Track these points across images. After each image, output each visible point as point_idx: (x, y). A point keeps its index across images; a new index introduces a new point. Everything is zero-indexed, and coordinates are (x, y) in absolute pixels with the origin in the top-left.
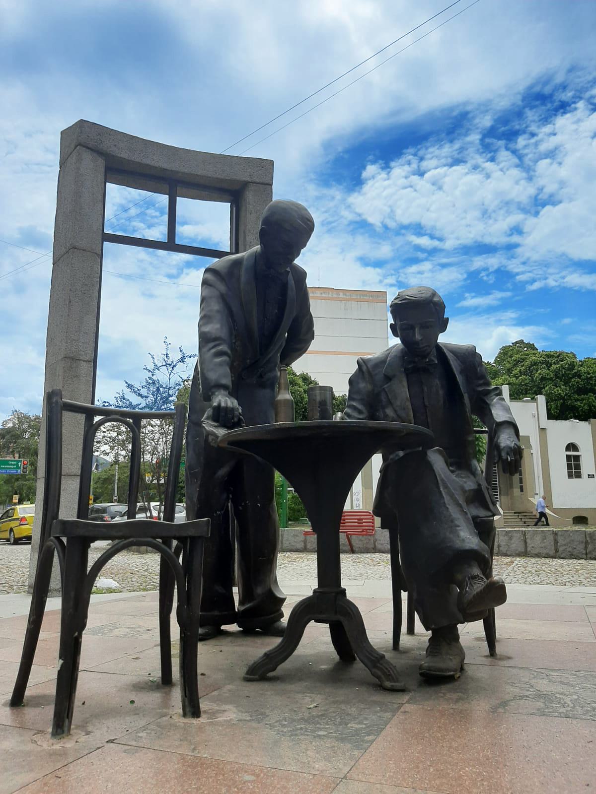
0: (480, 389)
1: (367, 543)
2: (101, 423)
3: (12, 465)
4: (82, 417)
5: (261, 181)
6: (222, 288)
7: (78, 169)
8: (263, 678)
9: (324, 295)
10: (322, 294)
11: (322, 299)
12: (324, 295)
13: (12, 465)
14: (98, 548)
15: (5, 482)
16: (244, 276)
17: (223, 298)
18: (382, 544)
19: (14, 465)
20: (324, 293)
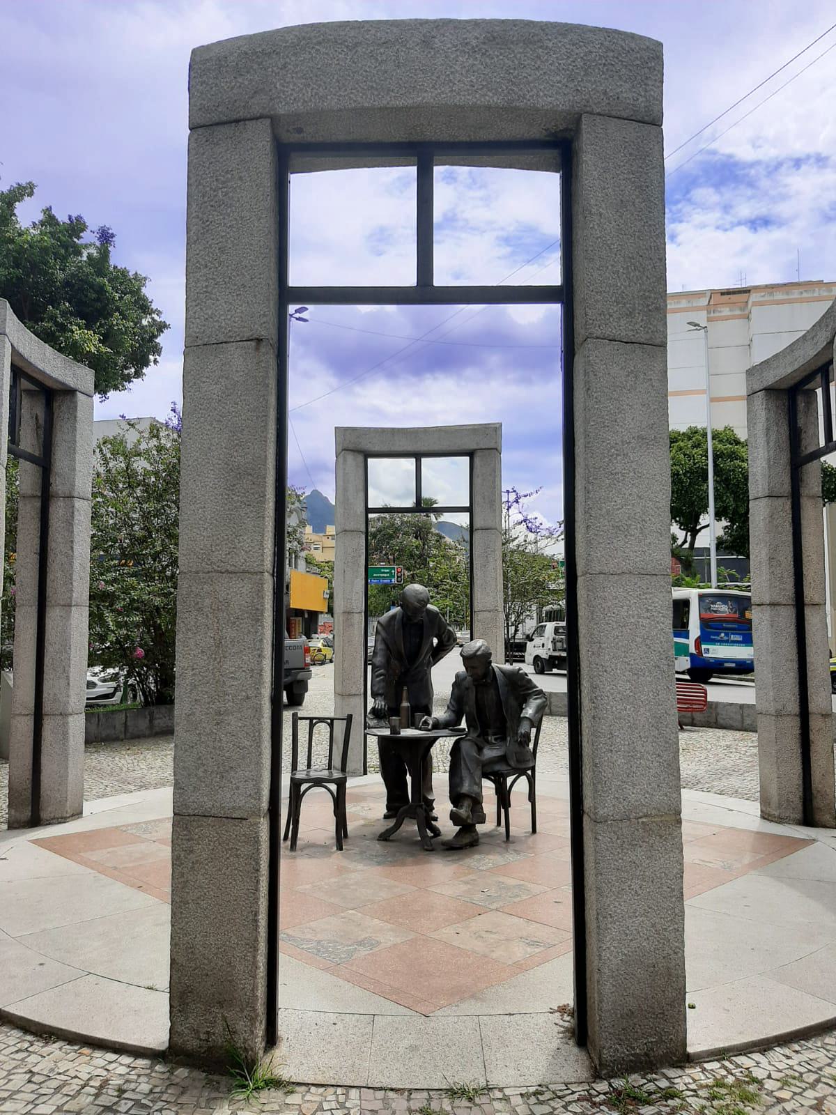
0: (522, 693)
1: (709, 717)
2: (316, 723)
3: (384, 573)
4: (308, 721)
5: (487, 447)
6: (383, 633)
7: (345, 469)
8: (386, 840)
9: (805, 295)
10: (802, 293)
11: (801, 301)
12: (805, 295)
13: (384, 573)
14: (304, 787)
15: (380, 591)
16: (397, 624)
17: (384, 640)
18: (724, 719)
19: (387, 573)
20: (805, 291)
